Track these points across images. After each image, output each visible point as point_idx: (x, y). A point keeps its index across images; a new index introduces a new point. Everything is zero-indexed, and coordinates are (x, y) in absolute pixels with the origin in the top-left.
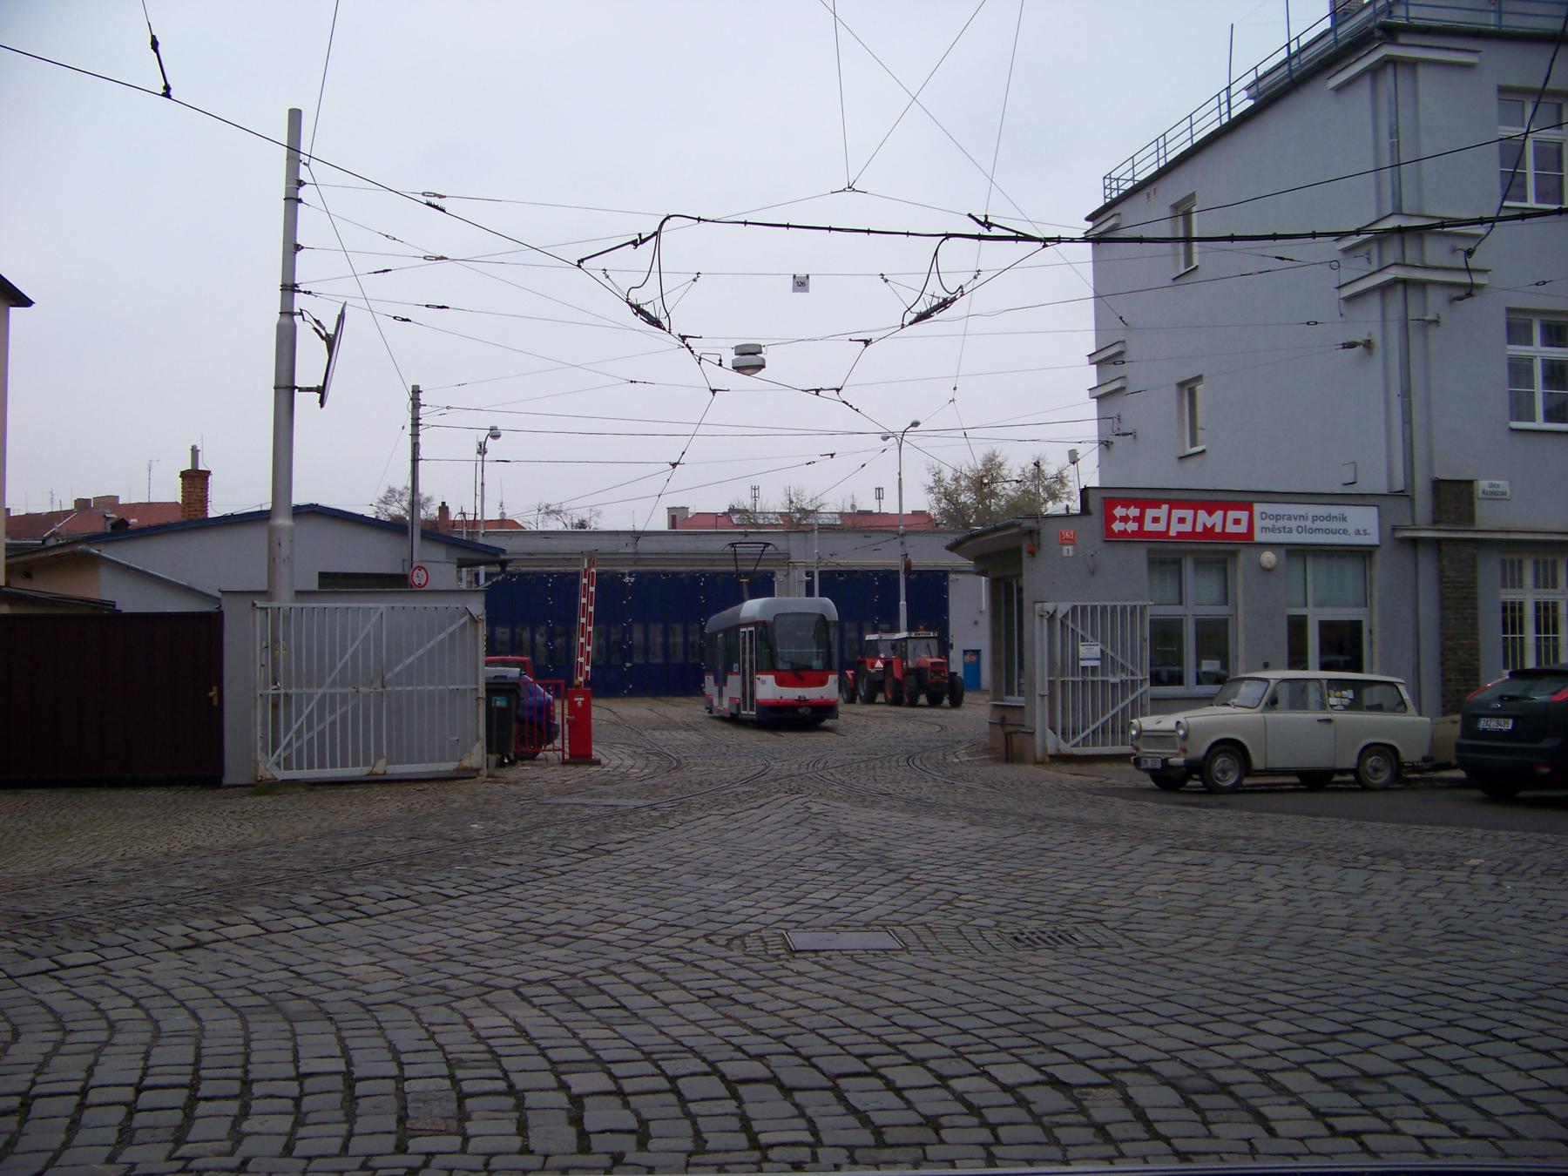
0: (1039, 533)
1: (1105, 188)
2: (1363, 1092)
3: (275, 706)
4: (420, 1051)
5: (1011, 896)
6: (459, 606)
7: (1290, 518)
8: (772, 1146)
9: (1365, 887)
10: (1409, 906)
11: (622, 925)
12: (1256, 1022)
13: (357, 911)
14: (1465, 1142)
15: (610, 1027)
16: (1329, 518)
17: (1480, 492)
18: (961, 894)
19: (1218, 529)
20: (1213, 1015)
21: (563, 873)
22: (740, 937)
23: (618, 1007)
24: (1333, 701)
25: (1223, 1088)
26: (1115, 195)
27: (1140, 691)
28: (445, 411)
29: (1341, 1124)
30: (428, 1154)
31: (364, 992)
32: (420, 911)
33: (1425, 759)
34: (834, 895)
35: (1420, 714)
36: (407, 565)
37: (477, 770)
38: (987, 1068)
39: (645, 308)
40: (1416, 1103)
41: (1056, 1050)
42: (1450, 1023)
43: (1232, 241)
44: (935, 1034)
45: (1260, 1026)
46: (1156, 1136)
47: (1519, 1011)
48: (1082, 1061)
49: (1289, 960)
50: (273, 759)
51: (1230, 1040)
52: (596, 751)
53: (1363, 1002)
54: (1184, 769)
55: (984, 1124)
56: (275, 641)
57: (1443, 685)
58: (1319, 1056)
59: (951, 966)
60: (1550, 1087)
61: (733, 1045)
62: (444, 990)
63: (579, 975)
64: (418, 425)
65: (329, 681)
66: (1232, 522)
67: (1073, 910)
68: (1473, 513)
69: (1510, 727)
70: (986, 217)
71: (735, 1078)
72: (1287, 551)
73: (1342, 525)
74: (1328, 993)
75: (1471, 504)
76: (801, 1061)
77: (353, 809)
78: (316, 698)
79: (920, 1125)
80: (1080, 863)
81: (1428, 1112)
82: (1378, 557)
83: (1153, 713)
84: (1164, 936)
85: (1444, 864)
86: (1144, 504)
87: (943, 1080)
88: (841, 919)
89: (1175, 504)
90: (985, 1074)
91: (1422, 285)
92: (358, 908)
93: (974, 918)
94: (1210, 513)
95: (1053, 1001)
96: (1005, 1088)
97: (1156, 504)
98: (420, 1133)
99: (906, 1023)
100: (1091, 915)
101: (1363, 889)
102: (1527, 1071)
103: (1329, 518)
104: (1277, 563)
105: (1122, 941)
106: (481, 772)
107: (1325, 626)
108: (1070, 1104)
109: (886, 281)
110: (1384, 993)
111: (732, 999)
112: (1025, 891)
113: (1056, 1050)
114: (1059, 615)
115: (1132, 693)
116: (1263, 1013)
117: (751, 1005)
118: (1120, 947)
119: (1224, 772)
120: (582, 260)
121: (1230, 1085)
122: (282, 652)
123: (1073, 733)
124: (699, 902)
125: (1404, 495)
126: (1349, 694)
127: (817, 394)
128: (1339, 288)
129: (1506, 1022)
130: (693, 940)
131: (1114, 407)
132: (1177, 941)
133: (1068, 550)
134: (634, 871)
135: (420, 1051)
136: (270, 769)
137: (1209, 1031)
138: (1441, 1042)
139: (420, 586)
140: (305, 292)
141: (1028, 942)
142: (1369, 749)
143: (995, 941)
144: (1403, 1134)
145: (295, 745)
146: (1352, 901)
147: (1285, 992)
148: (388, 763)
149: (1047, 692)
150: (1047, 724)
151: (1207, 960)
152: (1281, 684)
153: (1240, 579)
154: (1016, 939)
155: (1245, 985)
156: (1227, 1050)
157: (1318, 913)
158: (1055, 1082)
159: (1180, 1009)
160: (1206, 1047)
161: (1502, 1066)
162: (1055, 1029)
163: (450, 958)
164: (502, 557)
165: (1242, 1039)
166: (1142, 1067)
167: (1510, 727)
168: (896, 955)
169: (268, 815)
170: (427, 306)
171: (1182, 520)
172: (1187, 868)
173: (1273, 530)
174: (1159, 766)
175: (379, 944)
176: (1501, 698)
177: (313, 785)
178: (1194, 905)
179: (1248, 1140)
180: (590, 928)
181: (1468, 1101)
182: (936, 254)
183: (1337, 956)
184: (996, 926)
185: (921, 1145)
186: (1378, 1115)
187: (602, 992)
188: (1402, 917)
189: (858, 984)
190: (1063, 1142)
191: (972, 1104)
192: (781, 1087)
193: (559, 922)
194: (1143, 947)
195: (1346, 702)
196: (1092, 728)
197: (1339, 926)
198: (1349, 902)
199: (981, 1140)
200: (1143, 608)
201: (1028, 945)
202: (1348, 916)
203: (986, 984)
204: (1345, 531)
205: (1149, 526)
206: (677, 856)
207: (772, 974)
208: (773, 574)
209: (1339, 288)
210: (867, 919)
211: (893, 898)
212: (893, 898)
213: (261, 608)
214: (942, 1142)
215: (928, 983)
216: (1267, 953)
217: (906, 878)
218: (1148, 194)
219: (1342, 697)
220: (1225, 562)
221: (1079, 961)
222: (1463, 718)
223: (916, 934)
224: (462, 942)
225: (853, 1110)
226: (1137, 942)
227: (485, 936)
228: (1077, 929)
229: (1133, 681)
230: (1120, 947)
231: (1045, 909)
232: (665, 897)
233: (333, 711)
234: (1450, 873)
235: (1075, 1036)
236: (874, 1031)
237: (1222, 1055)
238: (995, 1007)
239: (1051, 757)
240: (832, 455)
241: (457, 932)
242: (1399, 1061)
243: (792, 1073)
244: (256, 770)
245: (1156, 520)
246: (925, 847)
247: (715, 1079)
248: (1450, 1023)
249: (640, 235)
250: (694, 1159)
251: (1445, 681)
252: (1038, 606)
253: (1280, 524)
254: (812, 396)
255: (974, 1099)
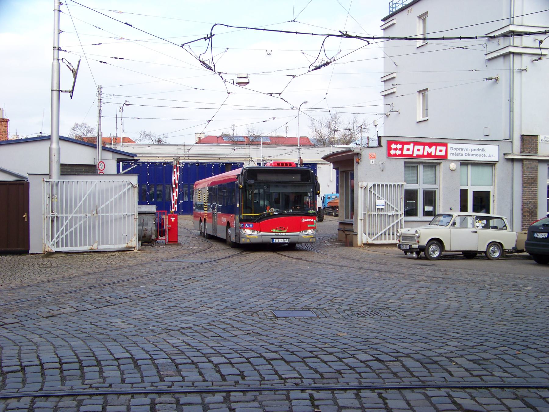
0: (361, 154)
1: (390, 7)
2: (483, 364)
3: (52, 221)
4: (154, 351)
5: (354, 298)
6: (127, 181)
7: (462, 150)
8: (287, 378)
9: (487, 297)
10: (503, 304)
11: (211, 308)
12: (447, 342)
13: (109, 303)
14: (516, 378)
15: (218, 343)
16: (478, 150)
17: (540, 140)
18: (335, 297)
19: (433, 154)
20: (432, 340)
21: (182, 289)
22: (256, 312)
23: (218, 337)
24: (478, 224)
25: (435, 362)
26: (394, 10)
27: (400, 218)
28: (112, 97)
29: (475, 373)
30: (172, 382)
31: (124, 332)
32: (133, 303)
33: (513, 248)
34: (288, 297)
35: (513, 231)
36: (96, 161)
37: (134, 247)
38: (354, 355)
39: (206, 62)
40: (501, 367)
41: (378, 350)
42: (514, 343)
43: (443, 40)
44: (335, 345)
45: (448, 343)
46: (414, 376)
47: (538, 340)
48: (387, 354)
49: (458, 322)
50: (51, 243)
51: (438, 348)
52: (180, 240)
53: (484, 336)
54: (418, 249)
55: (356, 372)
56: (52, 195)
57: (522, 218)
58: (468, 353)
59: (336, 323)
60: (545, 363)
61: (265, 348)
62: (153, 331)
63: (200, 326)
64: (101, 102)
65: (74, 211)
66: (439, 151)
67: (378, 304)
68: (537, 149)
69: (546, 237)
70: (346, 32)
71: (269, 358)
72: (461, 163)
73: (483, 153)
74: (472, 333)
75: (537, 145)
76: (290, 353)
77: (88, 263)
78: (69, 218)
79: (335, 372)
80: (380, 286)
81: (504, 370)
82: (497, 166)
83: (405, 227)
84: (413, 313)
85: (517, 289)
86: (403, 143)
87: (340, 359)
88: (292, 306)
89: (416, 144)
90: (354, 357)
91: (520, 54)
92: (109, 302)
93: (342, 306)
94: (430, 147)
95: (375, 335)
96: (361, 362)
97: (408, 143)
98: (167, 376)
99: (324, 341)
100: (385, 305)
101: (486, 298)
102: (538, 358)
103: (478, 150)
104: (457, 168)
105: (397, 315)
106: (136, 248)
107: (475, 193)
108: (384, 367)
109: (303, 53)
110: (492, 333)
111: (259, 334)
112: (359, 297)
113: (378, 350)
114: (369, 187)
115: (397, 219)
116: (449, 339)
117: (267, 336)
118: (397, 317)
119: (434, 252)
120: (183, 45)
121: (438, 361)
122: (55, 200)
123: (373, 235)
124: (237, 300)
125: (509, 140)
126: (484, 222)
127: (271, 95)
128: (486, 55)
129: (533, 343)
130: (238, 313)
131: (390, 99)
132: (417, 315)
133: (372, 161)
134: (209, 288)
135: (154, 351)
136: (50, 247)
137: (430, 345)
138: (510, 349)
139: (102, 170)
140: (64, 51)
141: (362, 315)
142: (491, 244)
143: (350, 314)
144: (495, 376)
145: (60, 237)
146: (482, 302)
147: (457, 333)
148: (99, 244)
149: (363, 219)
150: (363, 231)
151: (429, 321)
152: (457, 217)
153: (441, 173)
154: (358, 314)
155: (443, 330)
156: (436, 351)
157: (469, 306)
158: (378, 360)
159: (419, 338)
160: (429, 350)
161: (531, 357)
162: (376, 344)
163: (150, 320)
164: (135, 158)
165: (441, 348)
166: (408, 356)
167: (546, 237)
168: (315, 319)
169: (54, 266)
170: (115, 58)
171: (418, 150)
172: (420, 289)
173: (455, 154)
174: (408, 248)
175: (122, 315)
176: (544, 225)
177: (67, 253)
178: (423, 302)
179: (444, 378)
180: (198, 309)
181: (517, 367)
182: (324, 42)
183: (475, 321)
184: (350, 309)
185: (337, 378)
186: (487, 371)
187: (211, 331)
188: (500, 308)
189: (303, 328)
190: (383, 378)
191: (351, 367)
192: (285, 361)
193: (186, 307)
194: (405, 317)
195: (483, 225)
196: (381, 233)
197: (477, 310)
198: (481, 302)
199: (356, 377)
200: (402, 185)
201: (362, 316)
202: (480, 307)
203: (350, 329)
204: (484, 155)
205: (405, 152)
206: (224, 282)
207: (271, 325)
208: (243, 164)
209: (486, 55)
210: (302, 306)
211: (310, 298)
212: (310, 298)
213: (47, 182)
214: (343, 377)
215: (328, 328)
216: (451, 320)
217: (313, 291)
218: (408, 11)
219: (481, 223)
220: (436, 167)
221: (382, 321)
222: (528, 232)
223: (321, 312)
224: (153, 314)
225: (311, 368)
226: (402, 315)
227: (161, 312)
228: (380, 310)
229: (397, 214)
230: (397, 317)
231: (368, 303)
232: (224, 298)
233: (76, 224)
234: (519, 292)
235: (383, 346)
236: (313, 344)
237: (435, 352)
238: (354, 336)
239: (364, 244)
240: (274, 118)
241: (150, 310)
242: (496, 355)
243: (289, 357)
244: (45, 248)
245: (408, 150)
246: (319, 280)
247: (262, 359)
248: (514, 343)
249: (207, 35)
250: (262, 382)
251: (523, 216)
252: (360, 184)
253: (458, 152)
254: (269, 96)
255: (352, 365)
